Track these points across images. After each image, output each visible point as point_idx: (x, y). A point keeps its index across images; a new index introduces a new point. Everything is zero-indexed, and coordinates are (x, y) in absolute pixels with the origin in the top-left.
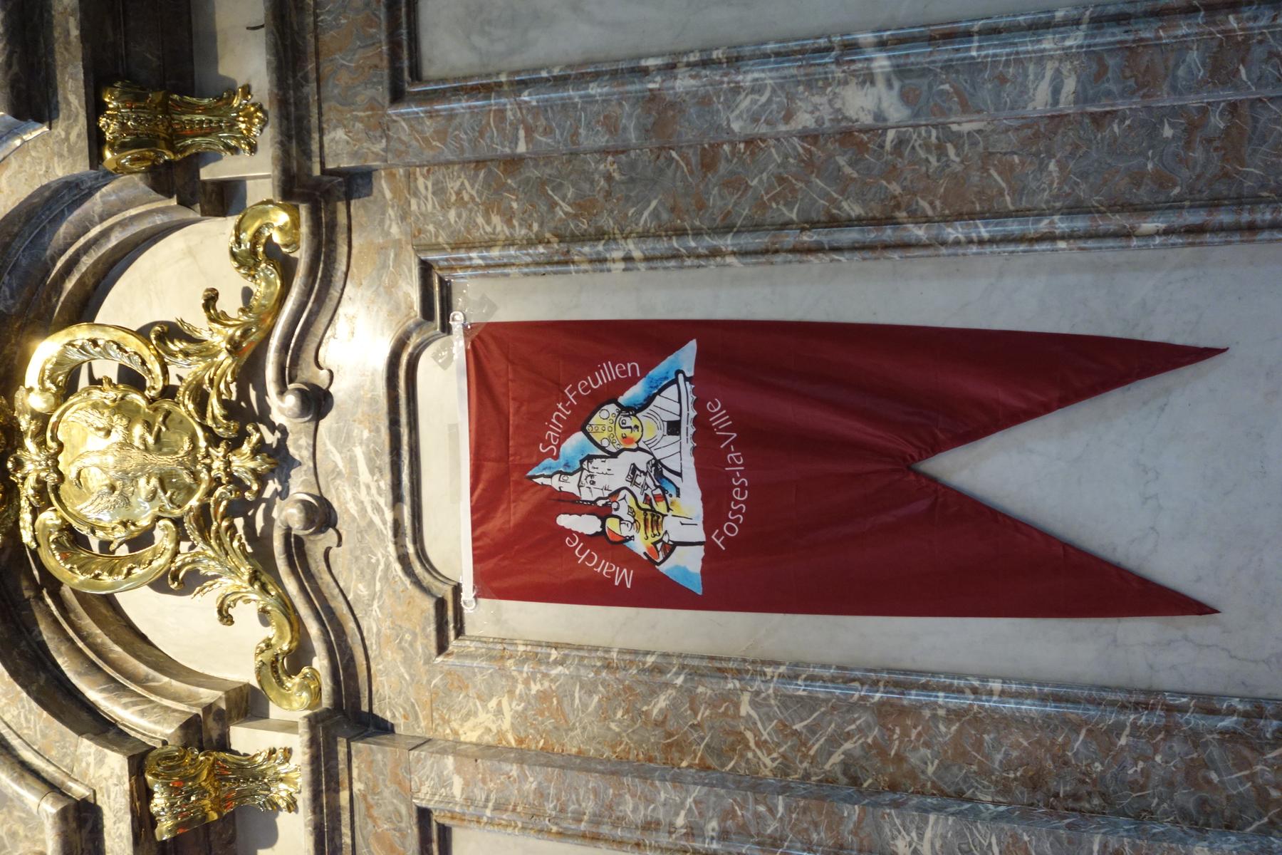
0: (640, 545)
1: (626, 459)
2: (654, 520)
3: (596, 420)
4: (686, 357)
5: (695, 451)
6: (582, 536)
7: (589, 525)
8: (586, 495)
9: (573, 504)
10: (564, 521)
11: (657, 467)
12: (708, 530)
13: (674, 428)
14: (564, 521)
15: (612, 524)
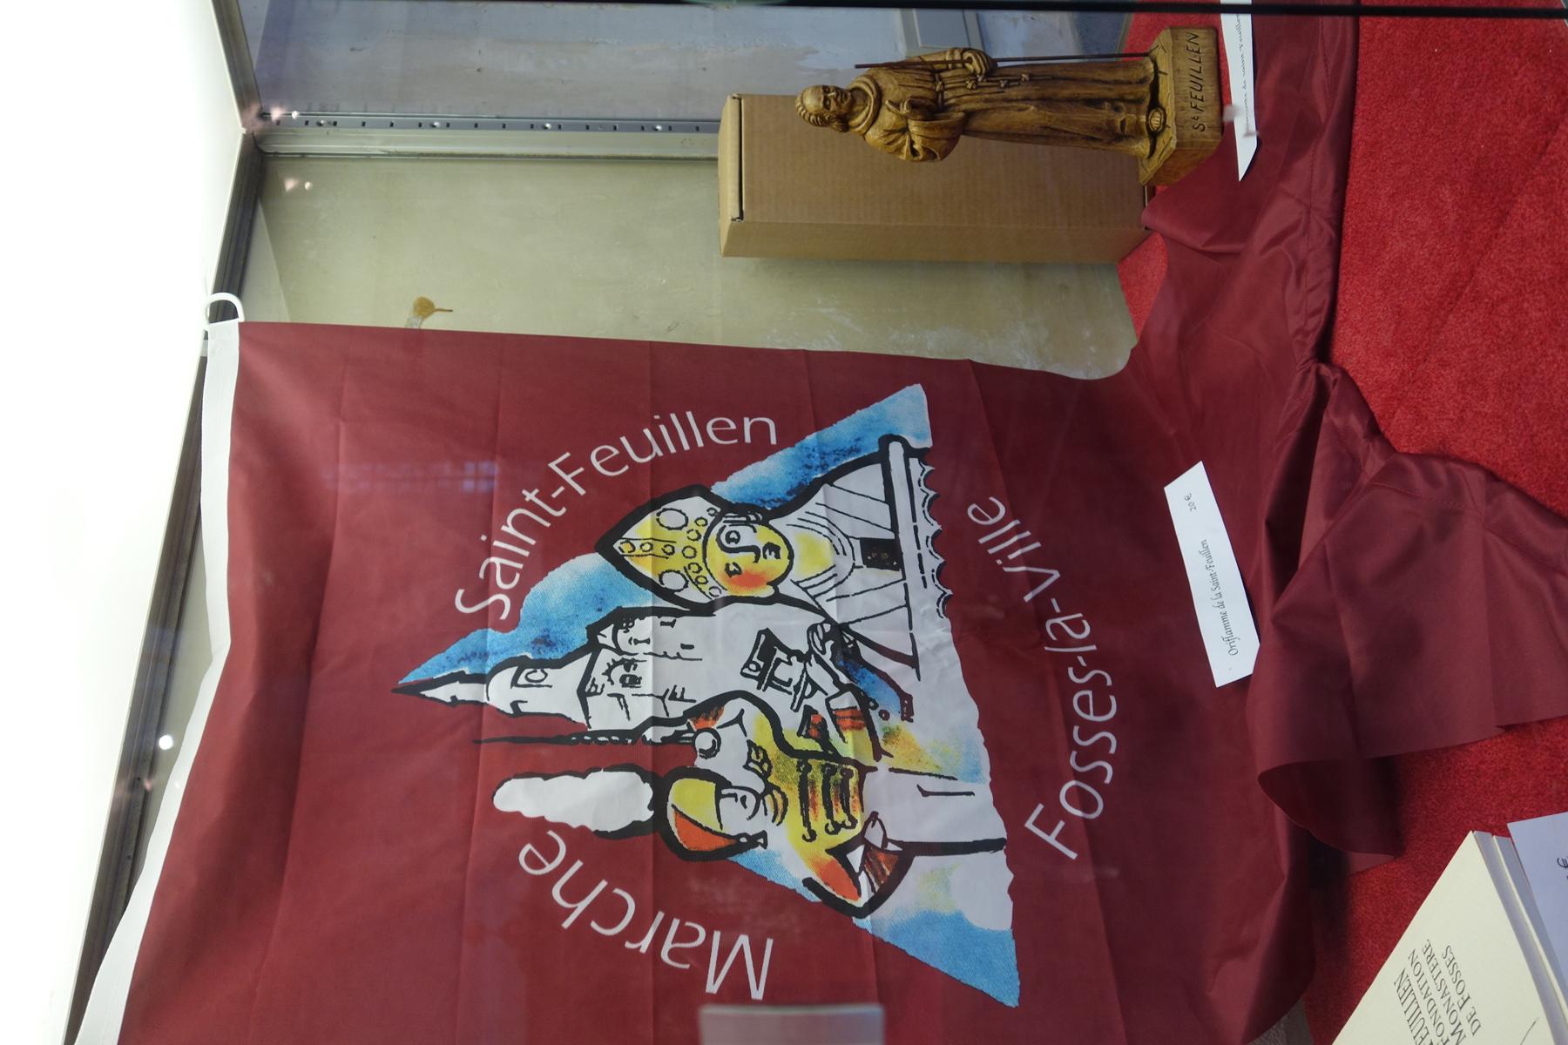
0: (791, 855)
1: (737, 629)
2: (829, 780)
3: (643, 529)
4: (908, 411)
5: (949, 607)
6: (582, 840)
7: (606, 800)
8: (605, 716)
9: (559, 747)
10: (519, 797)
11: (844, 645)
12: (1008, 801)
13: (882, 553)
14: (519, 797)
15: (690, 797)
